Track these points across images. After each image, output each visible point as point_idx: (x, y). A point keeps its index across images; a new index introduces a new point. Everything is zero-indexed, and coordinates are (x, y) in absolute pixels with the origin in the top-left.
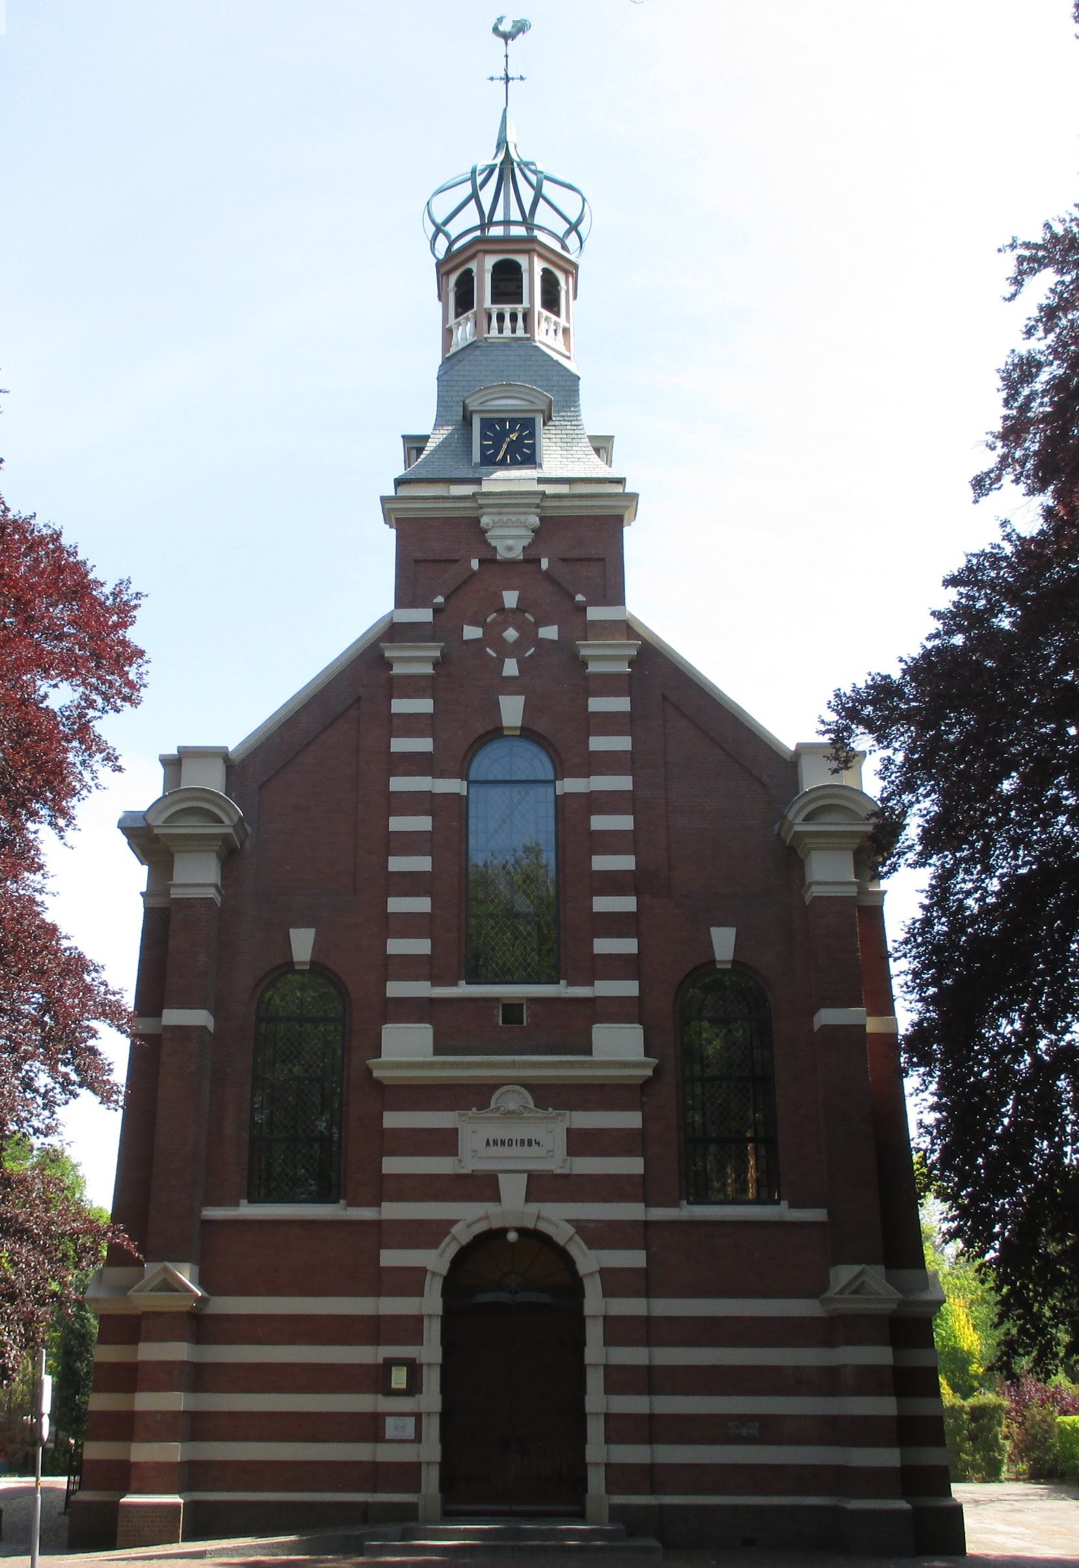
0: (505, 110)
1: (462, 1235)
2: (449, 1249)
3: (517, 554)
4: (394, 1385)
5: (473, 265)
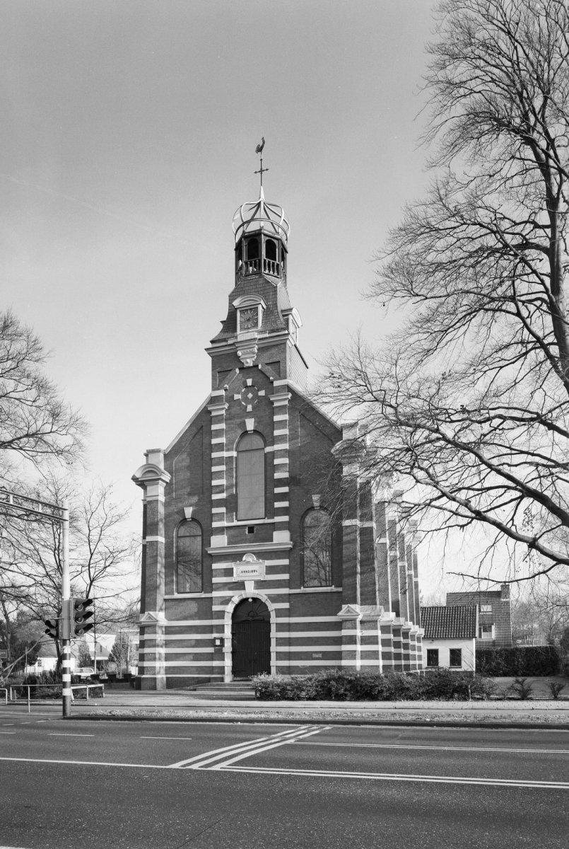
1: (236, 600)
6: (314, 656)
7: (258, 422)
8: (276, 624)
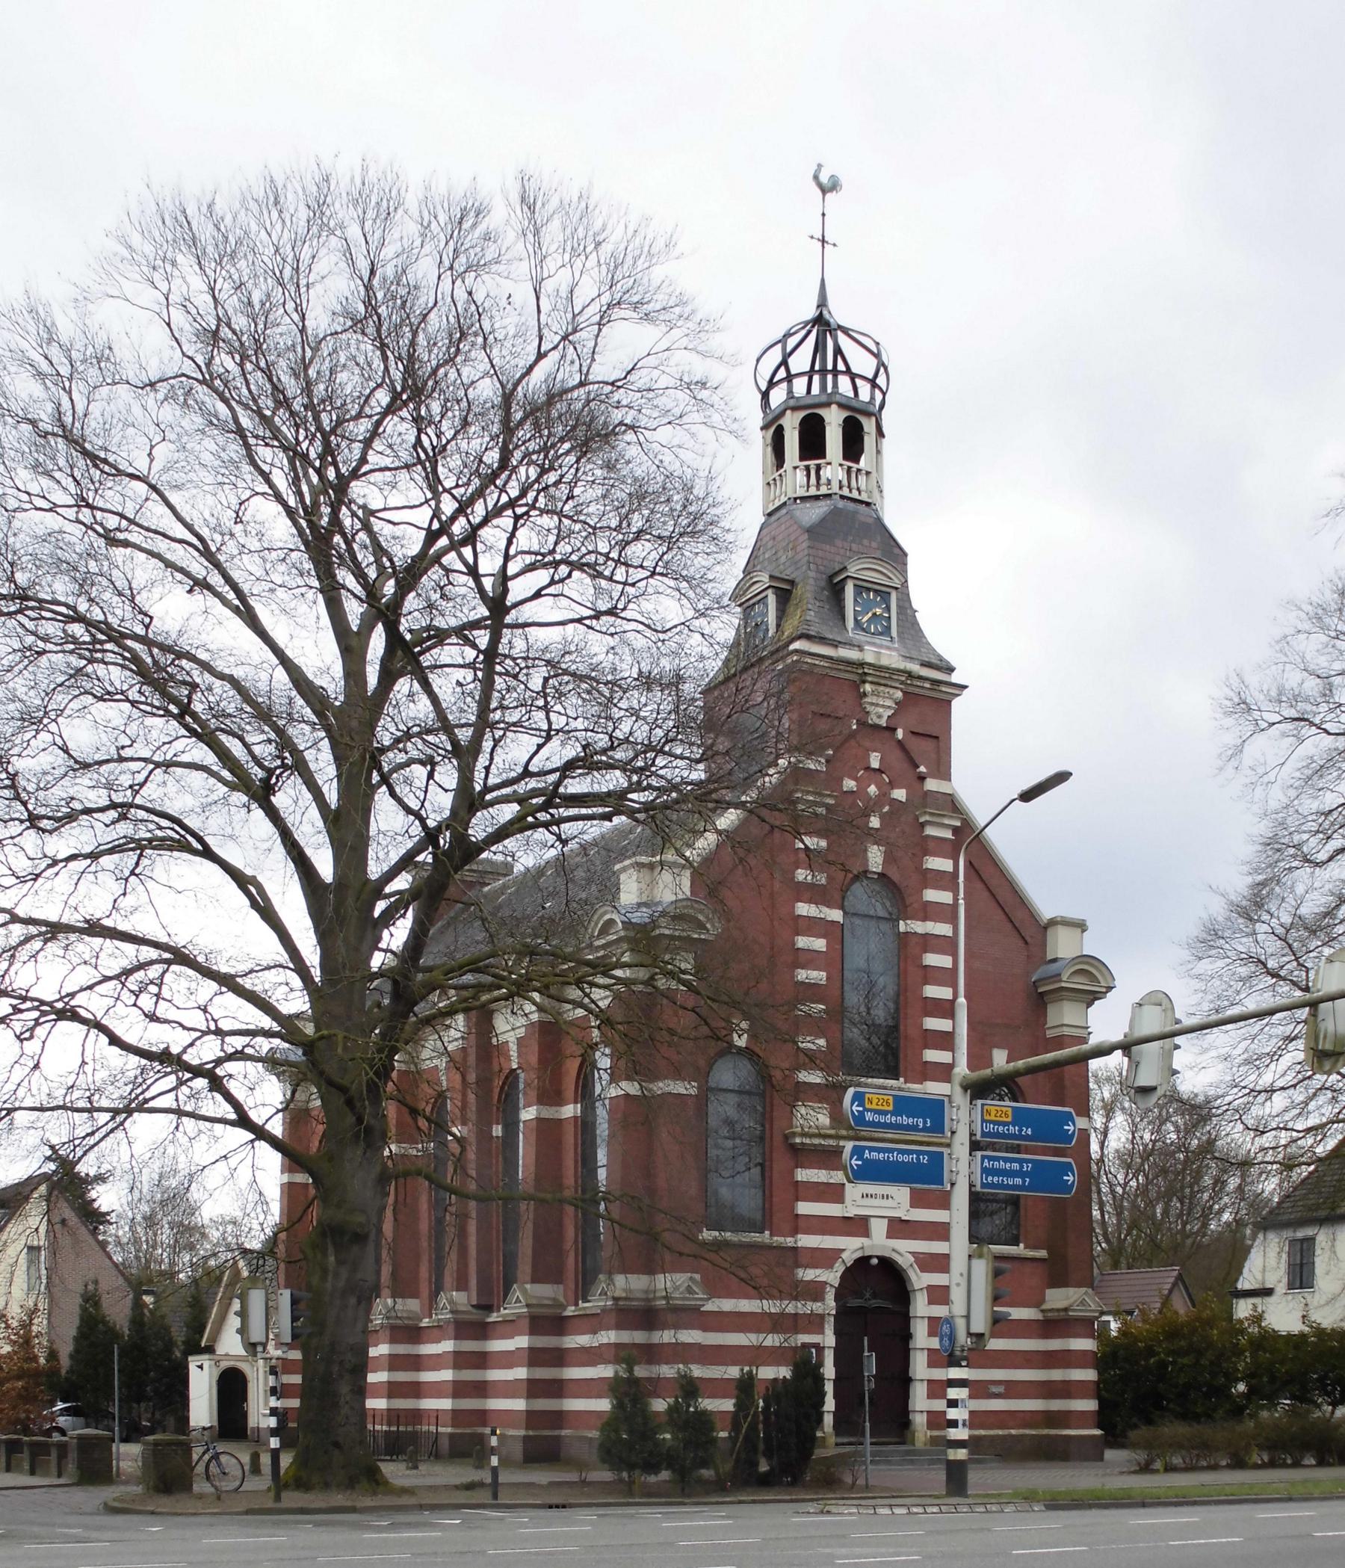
0: (823, 280)
1: (849, 1257)
2: (839, 1269)
3: (883, 722)
4: (950, 966)
5: (781, 422)
6: (995, 1389)
7: (889, 859)
8: (929, 1318)
